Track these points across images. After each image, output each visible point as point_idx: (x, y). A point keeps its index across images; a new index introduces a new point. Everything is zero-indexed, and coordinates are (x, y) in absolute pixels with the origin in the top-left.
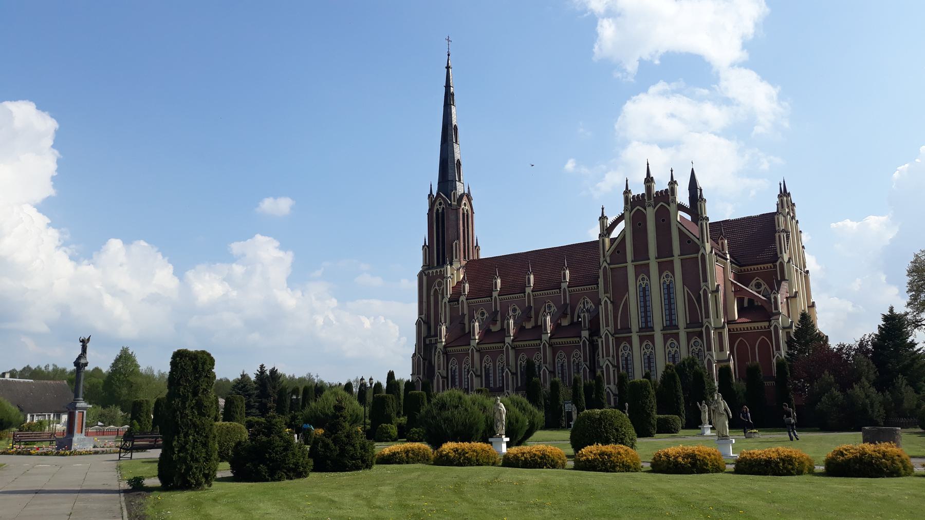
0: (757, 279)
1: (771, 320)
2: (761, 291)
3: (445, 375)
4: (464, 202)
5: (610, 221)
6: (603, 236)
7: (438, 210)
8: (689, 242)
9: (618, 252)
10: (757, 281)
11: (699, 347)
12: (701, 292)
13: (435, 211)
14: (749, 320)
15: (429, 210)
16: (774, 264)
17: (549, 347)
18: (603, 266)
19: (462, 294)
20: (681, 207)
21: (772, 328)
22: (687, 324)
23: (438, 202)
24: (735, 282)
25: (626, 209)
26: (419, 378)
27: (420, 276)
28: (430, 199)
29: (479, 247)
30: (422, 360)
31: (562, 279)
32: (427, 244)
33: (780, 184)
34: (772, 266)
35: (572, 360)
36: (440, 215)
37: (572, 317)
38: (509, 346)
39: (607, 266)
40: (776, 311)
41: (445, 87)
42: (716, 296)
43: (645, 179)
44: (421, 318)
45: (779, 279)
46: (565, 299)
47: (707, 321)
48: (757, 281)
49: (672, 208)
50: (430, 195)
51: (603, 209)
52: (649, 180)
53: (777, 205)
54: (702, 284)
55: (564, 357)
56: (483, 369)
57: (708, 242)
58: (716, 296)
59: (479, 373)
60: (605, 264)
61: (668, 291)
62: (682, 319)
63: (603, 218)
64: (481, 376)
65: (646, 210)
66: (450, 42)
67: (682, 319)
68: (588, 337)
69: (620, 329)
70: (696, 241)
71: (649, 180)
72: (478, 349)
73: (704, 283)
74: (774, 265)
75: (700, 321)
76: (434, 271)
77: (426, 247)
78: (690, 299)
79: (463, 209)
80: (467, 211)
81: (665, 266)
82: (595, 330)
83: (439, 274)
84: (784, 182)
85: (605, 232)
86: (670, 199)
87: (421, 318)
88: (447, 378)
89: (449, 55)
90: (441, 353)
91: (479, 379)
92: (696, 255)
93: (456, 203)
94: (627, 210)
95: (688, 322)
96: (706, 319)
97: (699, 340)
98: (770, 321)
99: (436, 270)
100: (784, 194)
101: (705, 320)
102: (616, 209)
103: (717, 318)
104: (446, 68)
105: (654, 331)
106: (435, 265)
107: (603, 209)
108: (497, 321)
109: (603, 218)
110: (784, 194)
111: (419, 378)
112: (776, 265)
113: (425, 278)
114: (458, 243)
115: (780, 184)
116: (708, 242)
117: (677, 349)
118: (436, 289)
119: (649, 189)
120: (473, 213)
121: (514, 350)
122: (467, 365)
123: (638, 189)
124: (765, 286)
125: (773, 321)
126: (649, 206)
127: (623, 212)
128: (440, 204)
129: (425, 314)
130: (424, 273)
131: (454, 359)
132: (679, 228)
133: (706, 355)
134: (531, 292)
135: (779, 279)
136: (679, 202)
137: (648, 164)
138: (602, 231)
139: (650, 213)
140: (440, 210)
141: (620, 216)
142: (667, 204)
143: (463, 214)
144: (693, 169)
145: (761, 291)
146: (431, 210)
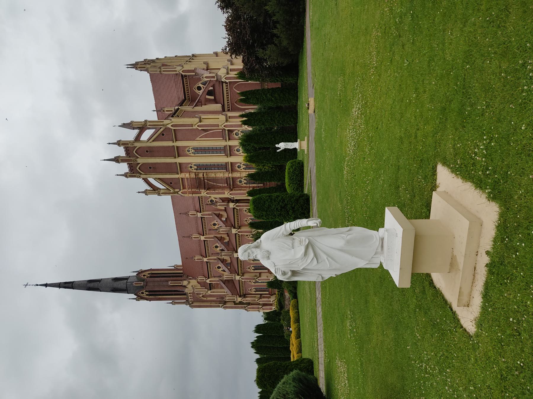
0: (195, 88)
1: (222, 82)
2: (203, 87)
3: (259, 296)
4: (142, 276)
5: (149, 188)
6: (159, 193)
7: (147, 295)
8: (163, 135)
9: (171, 183)
10: (196, 89)
11: (239, 132)
12: (200, 128)
13: (148, 297)
14: (144, 173)
15: (147, 300)
16: (184, 76)
17: (240, 229)
18: (181, 194)
19: (205, 281)
20: (138, 138)
21: (227, 81)
22: (223, 140)
23: (142, 295)
24: (195, 104)
25: (139, 177)
26: (261, 308)
27: (192, 307)
28: (139, 300)
29: (175, 265)
30: (249, 306)
31: (195, 216)
32: (171, 301)
33: (128, 68)
34: (186, 78)
35: (254, 284)
36: (151, 293)
37: (221, 210)
38: (241, 278)
39: (181, 191)
40: (215, 77)
41: (60, 288)
42: (203, 119)
43: (116, 162)
44: (222, 306)
45: (194, 74)
46: (209, 215)
47: (221, 126)
48: (196, 89)
49: (138, 145)
50: (137, 299)
51: (139, 192)
52: (117, 160)
53: (141, 70)
54: (194, 128)
55: (250, 266)
56: (256, 271)
57: (163, 122)
58: (203, 119)
59: (258, 274)
60: (180, 193)
61: (198, 151)
62: (220, 143)
63: (146, 192)
64: (260, 273)
65: (139, 163)
66: (28, 284)
67: (220, 143)
68: (234, 204)
69: (227, 185)
70: (162, 130)
71: (117, 160)
72: (242, 274)
73: (194, 126)
74: (185, 77)
75: (221, 130)
76: (190, 297)
77: (173, 303)
78: (206, 136)
79: (147, 277)
80: (149, 274)
81: (179, 152)
82: (229, 200)
83: (192, 297)
84: (127, 65)
85: (156, 192)
86: (131, 146)
87: (222, 306)
88: (261, 294)
89: (37, 285)
90: (244, 299)
91: (262, 274)
92: (173, 130)
93: (142, 283)
94: (139, 176)
95: (222, 139)
96: (219, 126)
97: (234, 132)
98: (222, 82)
99: (190, 299)
100: (136, 66)
101: (220, 128)
102: (138, 183)
103: (219, 118)
104: (46, 287)
105: (228, 162)
106: (186, 296)
107: (139, 192)
108: (223, 259)
109: (146, 192)
110: (136, 66)
111: (261, 308)
112: (185, 75)
113: (195, 304)
114: (171, 282)
115: (128, 68)
116: (163, 122)
117: (243, 179)
118: (202, 296)
119: (123, 161)
120: (151, 270)
121: (242, 227)
122: (250, 236)
123: (124, 167)
124: (200, 84)
125: (222, 80)
126: (136, 161)
127: (142, 179)
128: (143, 293)
129: (219, 303)
130: (191, 304)
131: (249, 290)
132: (153, 141)
133: (245, 128)
134: (204, 237)
135: (194, 74)
136: (134, 140)
137: (105, 160)
138: (156, 194)
139: (141, 160)
140: (147, 293)
141: (145, 181)
142: (196, 105)
143: (151, 277)
144: (119, 126)
145: (203, 87)
146: (147, 299)
